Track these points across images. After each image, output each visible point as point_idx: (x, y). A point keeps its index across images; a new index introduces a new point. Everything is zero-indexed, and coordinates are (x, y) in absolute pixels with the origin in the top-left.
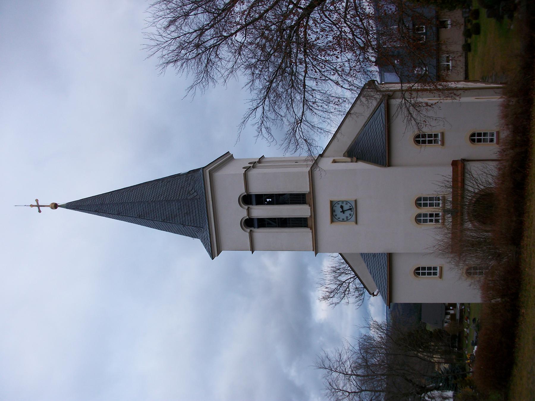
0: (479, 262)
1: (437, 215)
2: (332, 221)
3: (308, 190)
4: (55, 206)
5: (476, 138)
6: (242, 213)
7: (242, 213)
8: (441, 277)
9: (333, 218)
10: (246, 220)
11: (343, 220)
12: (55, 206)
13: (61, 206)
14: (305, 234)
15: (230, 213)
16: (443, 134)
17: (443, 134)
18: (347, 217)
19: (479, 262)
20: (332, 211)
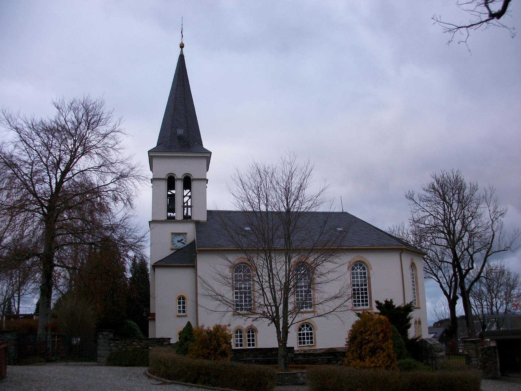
0: (23, 241)
1: (241, 345)
2: (172, 234)
3: (206, 220)
4: (182, 46)
5: (182, 301)
6: (179, 175)
7: (179, 175)
8: (178, 316)
9: (174, 234)
10: (174, 178)
11: (173, 241)
12: (182, 46)
13: (182, 50)
14: (163, 215)
15: (179, 167)
16: (186, 316)
17: (186, 316)
18: (175, 244)
19: (23, 241)
20: (179, 234)
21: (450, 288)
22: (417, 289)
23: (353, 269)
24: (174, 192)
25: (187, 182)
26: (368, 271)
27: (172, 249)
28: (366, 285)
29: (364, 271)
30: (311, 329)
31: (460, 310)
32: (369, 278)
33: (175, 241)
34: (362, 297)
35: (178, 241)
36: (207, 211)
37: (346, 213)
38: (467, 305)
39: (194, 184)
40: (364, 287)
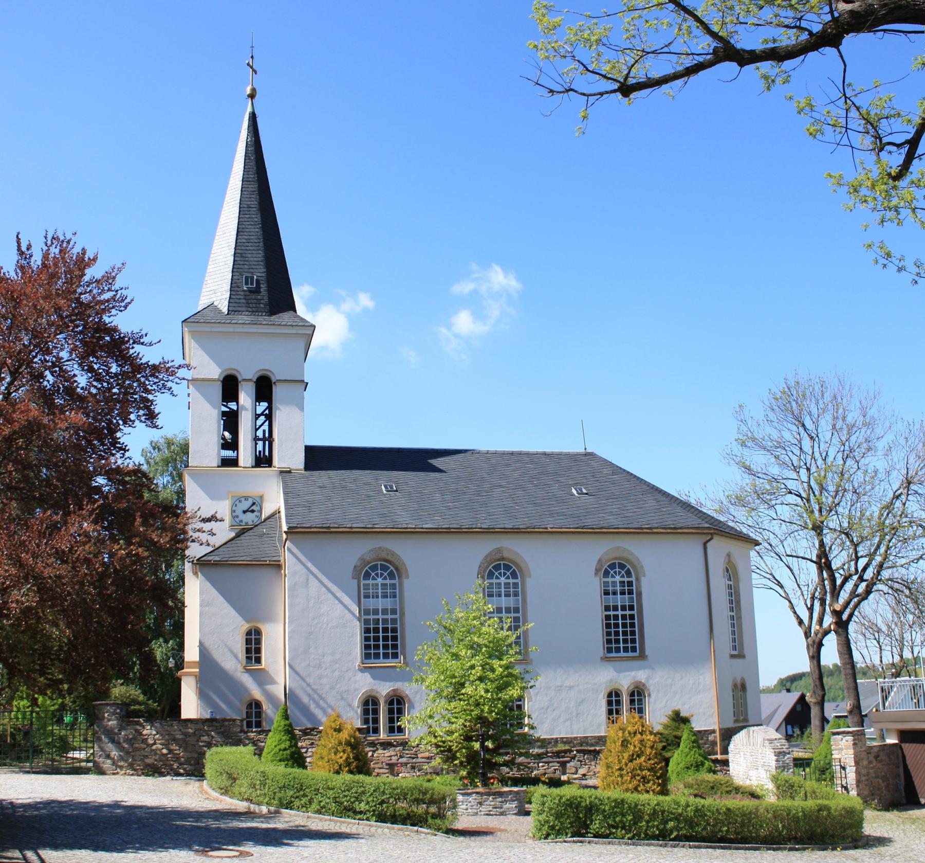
18: (237, 517)
21: (811, 610)
22: (739, 618)
23: (606, 574)
24: (233, 406)
25: (264, 388)
26: (637, 579)
27: (232, 530)
28: (631, 608)
29: (630, 579)
30: (514, 575)
31: (830, 655)
32: (639, 594)
33: (239, 512)
34: (625, 641)
35: (244, 512)
36: (307, 468)
37: (591, 454)
38: (846, 649)
39: (278, 392)
40: (628, 613)
